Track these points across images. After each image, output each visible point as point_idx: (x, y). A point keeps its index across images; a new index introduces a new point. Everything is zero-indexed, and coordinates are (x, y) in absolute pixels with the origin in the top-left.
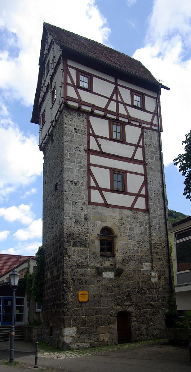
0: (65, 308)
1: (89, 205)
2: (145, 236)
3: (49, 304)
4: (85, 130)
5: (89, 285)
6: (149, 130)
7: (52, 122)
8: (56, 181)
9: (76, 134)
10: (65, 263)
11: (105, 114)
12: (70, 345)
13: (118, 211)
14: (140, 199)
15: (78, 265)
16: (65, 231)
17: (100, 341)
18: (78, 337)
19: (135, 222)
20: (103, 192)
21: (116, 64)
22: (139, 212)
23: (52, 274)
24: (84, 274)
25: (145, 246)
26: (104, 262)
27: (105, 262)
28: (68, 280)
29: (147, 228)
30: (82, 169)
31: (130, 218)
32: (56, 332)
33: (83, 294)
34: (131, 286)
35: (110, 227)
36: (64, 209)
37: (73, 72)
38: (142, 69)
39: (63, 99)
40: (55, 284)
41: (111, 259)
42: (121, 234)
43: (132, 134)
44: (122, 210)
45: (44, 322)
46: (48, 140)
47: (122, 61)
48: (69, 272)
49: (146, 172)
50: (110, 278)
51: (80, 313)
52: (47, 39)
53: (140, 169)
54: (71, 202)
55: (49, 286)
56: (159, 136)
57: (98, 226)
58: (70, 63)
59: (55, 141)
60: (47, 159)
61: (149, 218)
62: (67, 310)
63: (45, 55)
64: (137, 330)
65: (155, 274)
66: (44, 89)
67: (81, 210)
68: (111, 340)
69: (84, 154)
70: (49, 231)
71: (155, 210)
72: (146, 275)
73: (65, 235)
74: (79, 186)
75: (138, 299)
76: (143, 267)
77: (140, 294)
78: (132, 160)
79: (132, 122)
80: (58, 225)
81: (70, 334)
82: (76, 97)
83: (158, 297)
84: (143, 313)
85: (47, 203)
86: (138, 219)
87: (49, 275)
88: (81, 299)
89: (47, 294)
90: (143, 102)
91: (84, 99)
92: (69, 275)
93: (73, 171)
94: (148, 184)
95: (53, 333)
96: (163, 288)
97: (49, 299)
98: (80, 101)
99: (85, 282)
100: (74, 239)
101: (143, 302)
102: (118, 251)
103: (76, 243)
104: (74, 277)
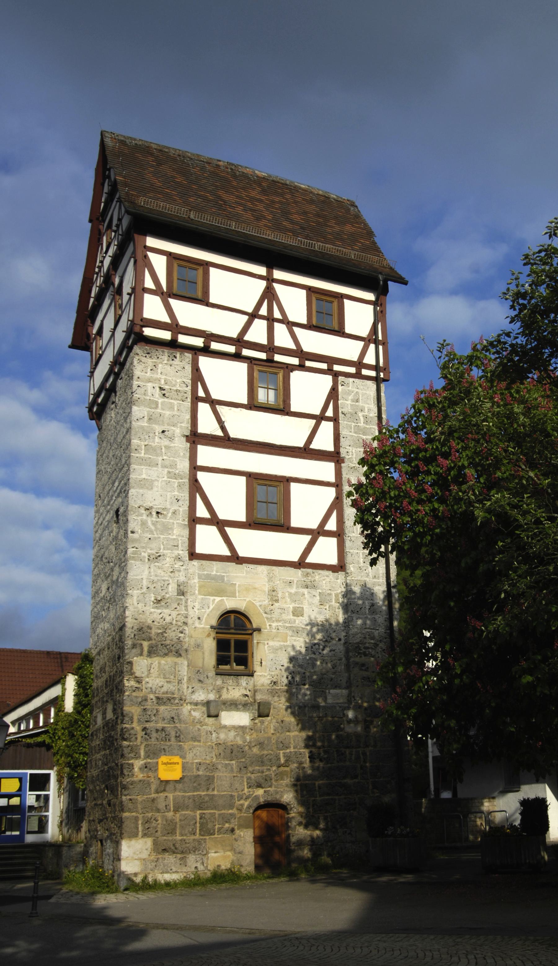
4: (186, 389)
79: (308, 364)
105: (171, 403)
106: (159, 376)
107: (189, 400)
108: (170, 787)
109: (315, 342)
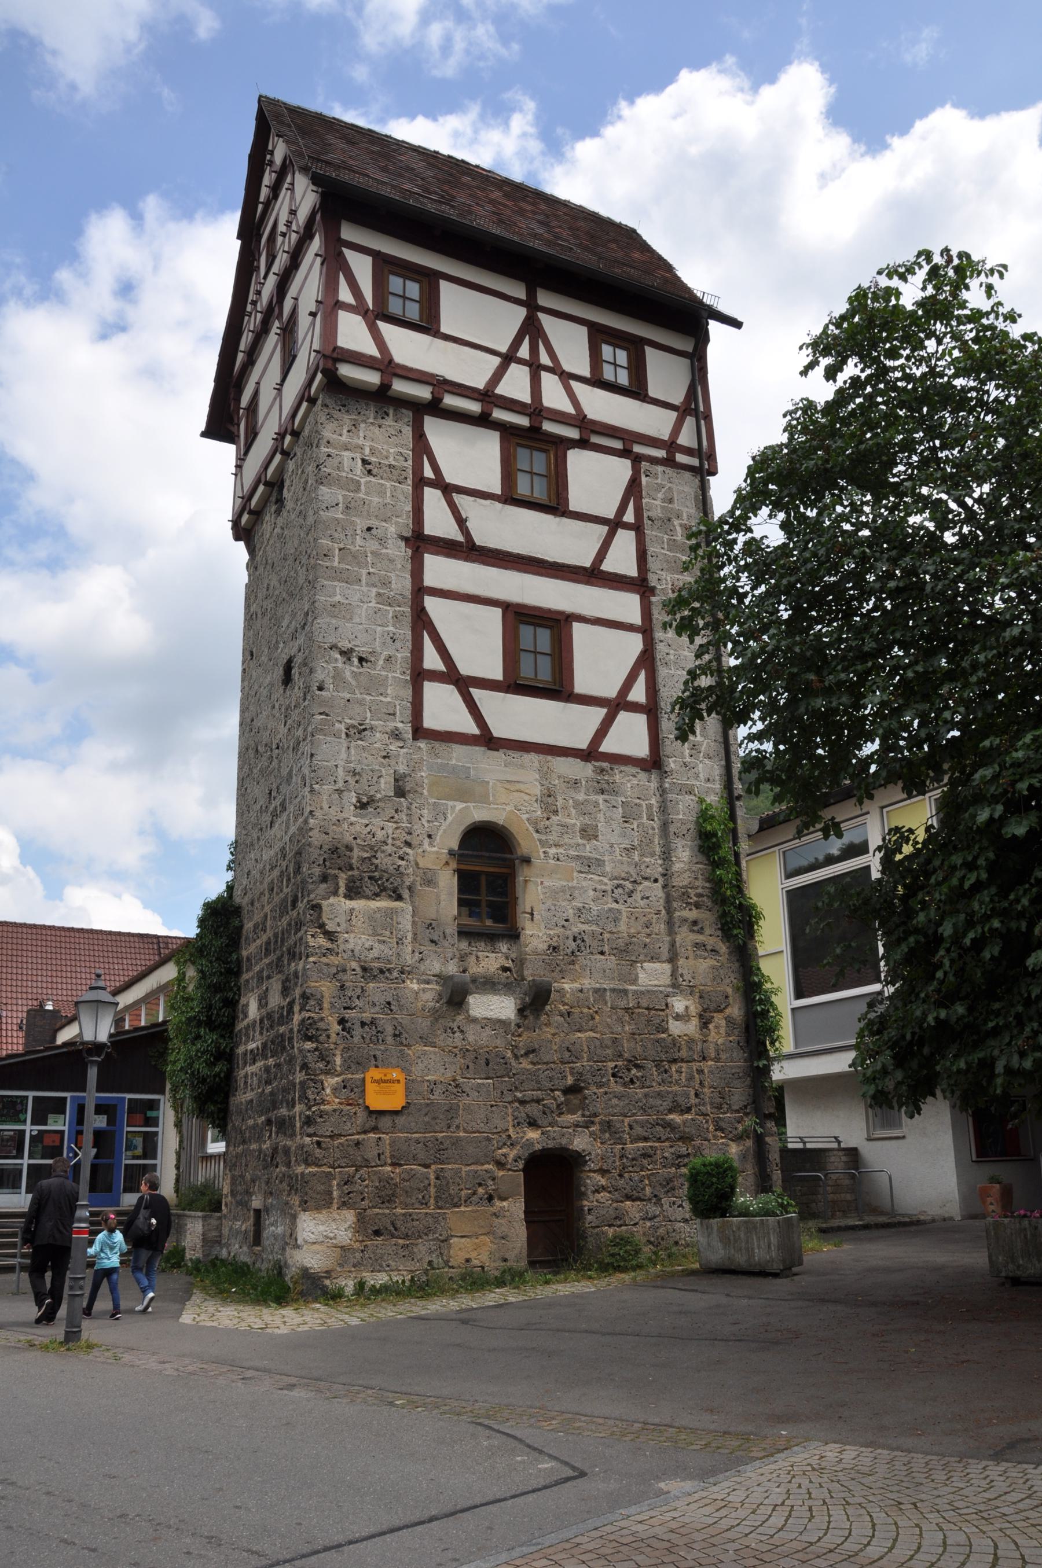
0: (309, 1136)
1: (414, 739)
2: (647, 860)
3: (251, 1122)
5: (409, 1046)
7: (280, 436)
8: (286, 651)
9: (369, 479)
10: (311, 959)
11: (484, 410)
12: (327, 1282)
13: (536, 764)
14: (623, 717)
15: (364, 969)
16: (316, 837)
17: (453, 1267)
18: (362, 1251)
19: (602, 806)
20: (476, 693)
21: (535, 236)
22: (623, 768)
23: (264, 1002)
24: (389, 1003)
25: (647, 898)
26: (473, 958)
27: (477, 957)
29: (653, 829)
30: (390, 605)
31: (583, 790)
32: (273, 1228)
33: (386, 1082)
34: (586, 1049)
35: (501, 822)
36: (312, 755)
37: (362, 267)
38: (637, 255)
39: (319, 356)
40: (273, 1042)
41: (504, 947)
42: (545, 852)
43: (595, 479)
44: (549, 758)
45: (232, 1191)
46: (265, 501)
47: (560, 227)
48: (326, 995)
49: (651, 620)
50: (500, 1021)
51: (371, 1154)
52: (272, 153)
53: (627, 606)
54: (342, 727)
55: (252, 1051)
56: (704, 488)
57: (450, 818)
58: (348, 232)
59: (289, 504)
60: (261, 569)
61: (662, 791)
62: (319, 1143)
63: (260, 206)
64: (610, 1226)
65: (687, 1007)
66: (252, 322)
67: (384, 757)
69: (400, 552)
70: (258, 838)
71: (688, 759)
72: (647, 1009)
73: (314, 853)
74: (379, 668)
75: (615, 1101)
76: (636, 979)
77: (625, 1085)
78: (593, 575)
79: (595, 439)
80: (289, 815)
81: (327, 1237)
82: (372, 350)
83: (697, 1095)
84: (633, 1159)
85: (252, 734)
86: (614, 792)
87: (253, 1011)
88: (376, 1100)
89: (246, 1083)
90: (638, 369)
91: (399, 357)
92: (326, 1005)
93: (359, 613)
94: (659, 663)
95: (265, 1234)
96: (717, 1059)
97: (252, 1101)
98: (387, 366)
99: (395, 1035)
100: (351, 868)
101: (634, 1115)
102: (532, 914)
103: (358, 884)
104: (349, 1014)
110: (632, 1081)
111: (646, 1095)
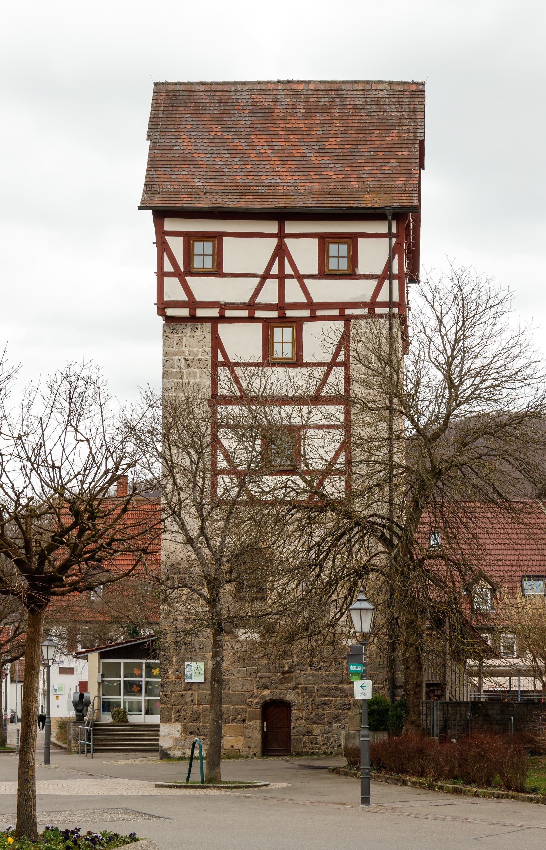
4: (207, 357)
6: (365, 320)
28: (167, 645)
51: (188, 700)
62: (166, 695)
68: (247, 749)
79: (319, 313)
105: (195, 372)
106: (183, 349)
107: (210, 366)
108: (195, 687)
109: (324, 291)
110: (320, 668)
111: (328, 675)
